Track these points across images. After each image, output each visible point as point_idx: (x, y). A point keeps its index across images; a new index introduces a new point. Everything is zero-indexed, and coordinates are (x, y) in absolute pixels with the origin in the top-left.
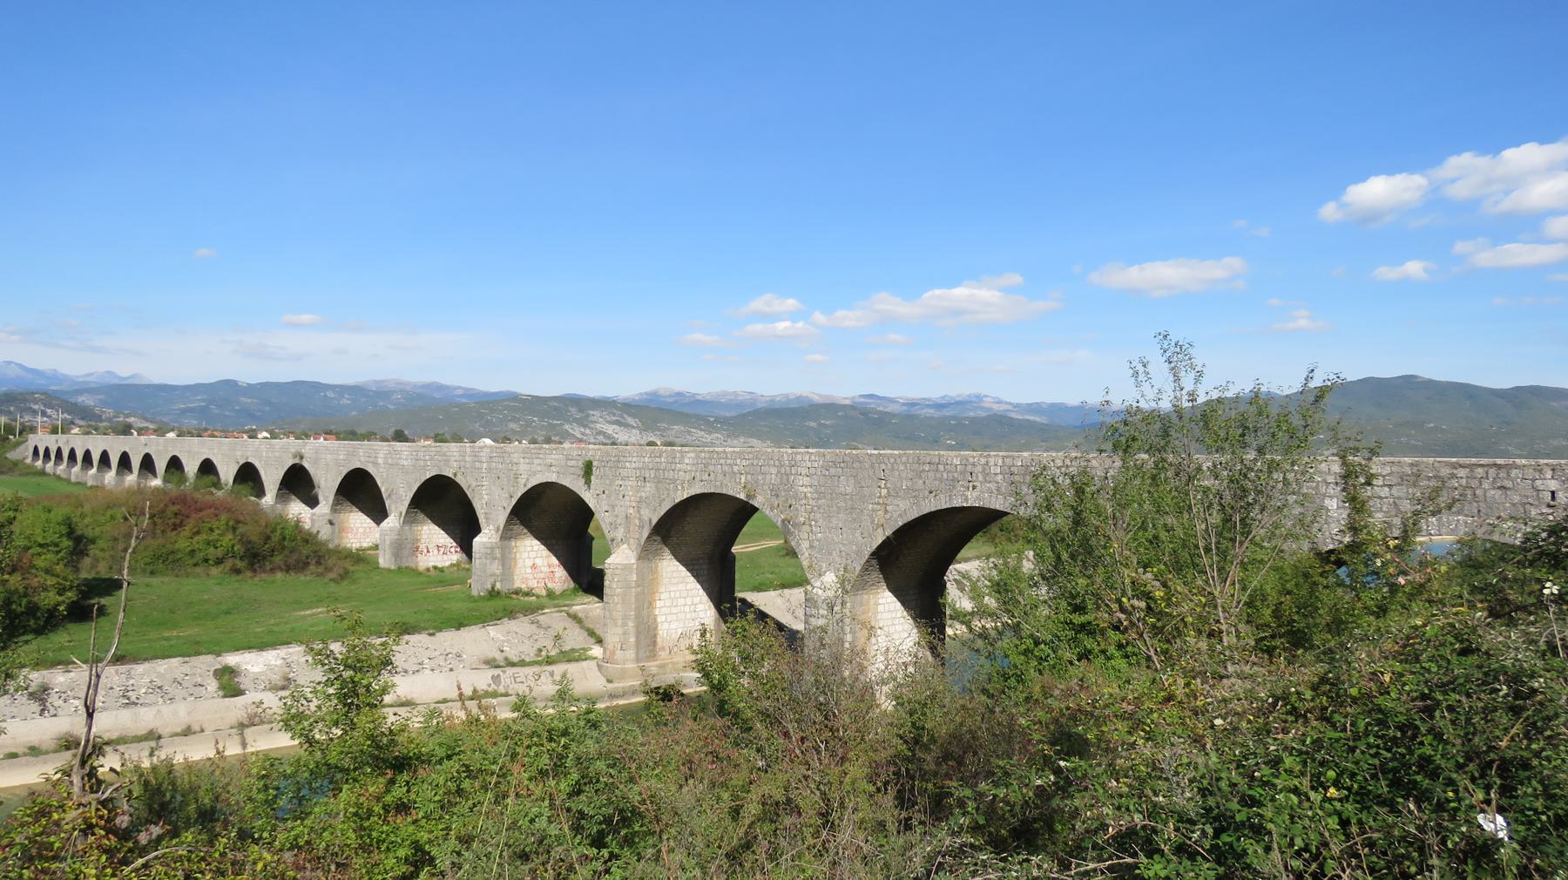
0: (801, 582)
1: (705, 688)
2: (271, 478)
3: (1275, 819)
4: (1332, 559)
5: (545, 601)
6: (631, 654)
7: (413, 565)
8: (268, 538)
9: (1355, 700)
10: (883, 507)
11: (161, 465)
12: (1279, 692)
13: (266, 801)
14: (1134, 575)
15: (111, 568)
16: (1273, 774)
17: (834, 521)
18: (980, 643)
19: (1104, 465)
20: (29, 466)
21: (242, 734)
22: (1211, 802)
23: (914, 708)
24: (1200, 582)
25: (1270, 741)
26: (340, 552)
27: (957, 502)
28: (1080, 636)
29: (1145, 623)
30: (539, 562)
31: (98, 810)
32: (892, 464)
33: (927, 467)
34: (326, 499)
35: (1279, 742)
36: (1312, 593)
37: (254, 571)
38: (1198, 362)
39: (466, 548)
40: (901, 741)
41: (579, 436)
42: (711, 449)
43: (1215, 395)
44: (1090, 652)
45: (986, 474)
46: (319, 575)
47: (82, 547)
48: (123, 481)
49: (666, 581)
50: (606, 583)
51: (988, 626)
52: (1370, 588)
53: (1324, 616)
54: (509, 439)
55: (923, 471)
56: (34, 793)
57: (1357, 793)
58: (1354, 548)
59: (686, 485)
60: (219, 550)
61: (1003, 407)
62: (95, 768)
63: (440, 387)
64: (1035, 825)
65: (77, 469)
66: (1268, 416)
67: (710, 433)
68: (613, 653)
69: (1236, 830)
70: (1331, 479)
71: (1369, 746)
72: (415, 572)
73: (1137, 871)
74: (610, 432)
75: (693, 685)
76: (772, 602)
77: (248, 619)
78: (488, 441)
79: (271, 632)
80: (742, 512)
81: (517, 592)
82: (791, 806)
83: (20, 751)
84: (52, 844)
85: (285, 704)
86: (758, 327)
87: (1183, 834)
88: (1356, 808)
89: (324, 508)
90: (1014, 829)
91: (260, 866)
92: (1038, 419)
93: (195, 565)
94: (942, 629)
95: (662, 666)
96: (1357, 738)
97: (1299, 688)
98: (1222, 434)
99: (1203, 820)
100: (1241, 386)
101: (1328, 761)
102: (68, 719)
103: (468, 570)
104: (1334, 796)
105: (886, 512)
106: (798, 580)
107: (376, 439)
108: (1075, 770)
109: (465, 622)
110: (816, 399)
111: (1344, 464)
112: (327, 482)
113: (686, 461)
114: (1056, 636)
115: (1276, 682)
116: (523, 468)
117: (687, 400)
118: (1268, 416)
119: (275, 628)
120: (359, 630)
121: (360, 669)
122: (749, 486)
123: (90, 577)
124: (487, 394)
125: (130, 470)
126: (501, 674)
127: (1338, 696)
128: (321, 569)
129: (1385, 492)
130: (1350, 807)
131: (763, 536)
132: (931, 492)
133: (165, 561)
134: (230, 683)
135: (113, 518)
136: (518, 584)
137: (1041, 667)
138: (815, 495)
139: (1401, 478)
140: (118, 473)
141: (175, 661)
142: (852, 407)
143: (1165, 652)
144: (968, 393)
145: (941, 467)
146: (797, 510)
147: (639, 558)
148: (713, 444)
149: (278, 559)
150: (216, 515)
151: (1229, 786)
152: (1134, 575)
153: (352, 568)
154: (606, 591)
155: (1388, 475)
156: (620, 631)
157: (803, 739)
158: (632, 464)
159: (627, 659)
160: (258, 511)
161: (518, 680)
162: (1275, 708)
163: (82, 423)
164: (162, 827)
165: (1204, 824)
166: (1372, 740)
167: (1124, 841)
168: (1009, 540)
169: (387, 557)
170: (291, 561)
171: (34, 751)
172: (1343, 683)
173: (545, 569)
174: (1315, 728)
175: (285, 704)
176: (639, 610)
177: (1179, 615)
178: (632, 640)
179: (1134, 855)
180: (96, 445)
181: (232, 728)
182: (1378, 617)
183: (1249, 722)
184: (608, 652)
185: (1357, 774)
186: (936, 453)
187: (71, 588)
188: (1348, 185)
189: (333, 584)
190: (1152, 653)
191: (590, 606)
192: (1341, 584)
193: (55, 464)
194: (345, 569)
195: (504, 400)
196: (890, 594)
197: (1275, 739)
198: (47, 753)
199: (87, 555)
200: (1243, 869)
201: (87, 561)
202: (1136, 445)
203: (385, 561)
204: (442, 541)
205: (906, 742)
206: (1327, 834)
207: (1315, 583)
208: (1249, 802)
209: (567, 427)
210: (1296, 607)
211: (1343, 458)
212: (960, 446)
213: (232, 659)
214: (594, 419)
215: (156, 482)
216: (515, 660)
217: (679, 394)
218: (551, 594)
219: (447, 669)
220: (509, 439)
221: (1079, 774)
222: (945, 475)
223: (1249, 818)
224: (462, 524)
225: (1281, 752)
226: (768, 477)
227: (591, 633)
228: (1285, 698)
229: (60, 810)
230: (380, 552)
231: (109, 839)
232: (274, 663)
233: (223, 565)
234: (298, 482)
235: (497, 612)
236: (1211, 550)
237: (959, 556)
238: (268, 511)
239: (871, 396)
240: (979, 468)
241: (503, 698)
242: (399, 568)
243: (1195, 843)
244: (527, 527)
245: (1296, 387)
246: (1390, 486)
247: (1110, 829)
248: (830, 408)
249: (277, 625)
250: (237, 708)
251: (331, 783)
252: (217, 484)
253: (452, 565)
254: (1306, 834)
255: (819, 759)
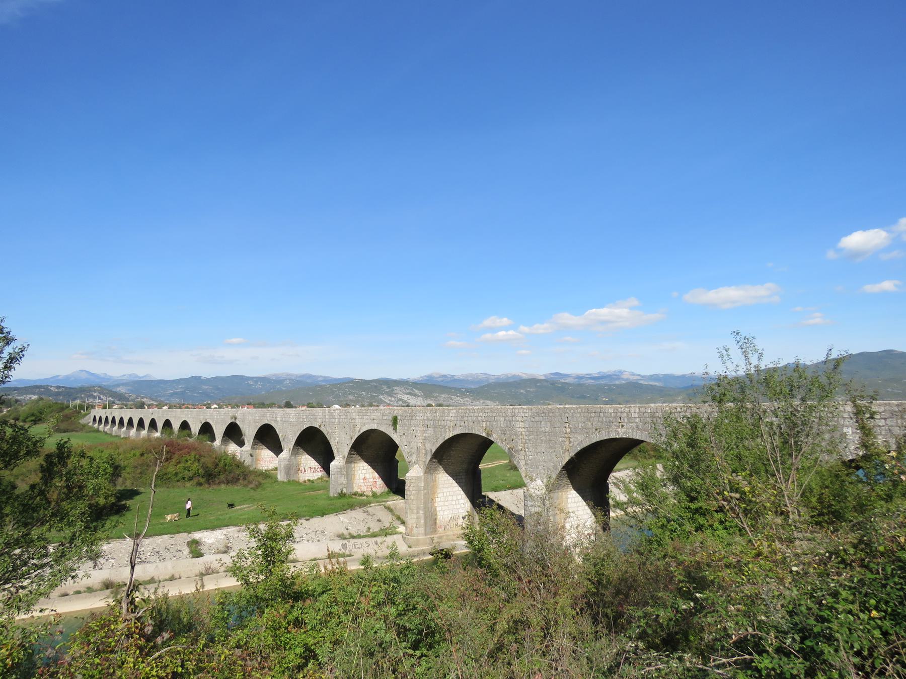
0: (521, 485)
1: (470, 550)
2: (219, 431)
3: (840, 631)
4: (852, 465)
5: (371, 499)
6: (422, 530)
7: (296, 479)
8: (217, 465)
9: (882, 554)
10: (568, 440)
11: (160, 425)
12: (832, 549)
13: (223, 618)
14: (730, 477)
15: (133, 484)
16: (835, 602)
17: (539, 449)
18: (633, 522)
19: (707, 411)
20: (91, 427)
21: (202, 580)
22: (797, 619)
23: (597, 563)
24: (772, 482)
25: (830, 581)
26: (256, 472)
27: (613, 435)
28: (696, 516)
29: (740, 507)
30: (367, 476)
31: (135, 623)
32: (572, 413)
33: (593, 415)
34: (249, 441)
35: (835, 581)
36: (842, 487)
37: (209, 484)
38: (759, 347)
39: (326, 469)
40: (590, 583)
41: (388, 402)
42: (465, 408)
43: (771, 366)
44: (702, 526)
45: (629, 418)
46: (246, 486)
47: (117, 472)
48: (140, 434)
49: (441, 486)
50: (407, 488)
51: (637, 510)
52: (880, 483)
53: (851, 502)
54: (349, 405)
55: (591, 417)
56: (93, 614)
57: (891, 614)
58: (865, 458)
59: (451, 429)
60: (191, 472)
61: (635, 378)
62: (134, 599)
63: (310, 376)
64: (677, 636)
65: (116, 428)
66: (805, 379)
67: (463, 398)
68: (411, 530)
69: (815, 638)
70: (846, 415)
71: (895, 584)
72: (297, 483)
73: (753, 664)
74: (405, 399)
75: (461, 548)
76: (504, 498)
77: (206, 512)
78: (337, 406)
79: (218, 519)
80: (483, 444)
81: (355, 494)
82: (527, 624)
83: (82, 590)
84: (110, 643)
85: (233, 561)
86: (488, 336)
87: (780, 640)
88: (892, 624)
89: (247, 447)
90: (664, 639)
91: (223, 657)
92: (657, 384)
93: (178, 481)
94: (606, 512)
95: (440, 538)
96: (887, 579)
97: (845, 547)
98: (778, 389)
99: (793, 631)
100: (787, 359)
101: (870, 594)
102: (108, 571)
103: (327, 481)
104: (876, 616)
105: (570, 442)
106: (518, 484)
107: (275, 407)
108: (707, 599)
109: (327, 512)
110: (525, 377)
111: (855, 406)
112: (249, 432)
113: (451, 415)
114: (680, 516)
115: (829, 543)
116: (358, 421)
117: (449, 380)
118: (805, 379)
119: (221, 517)
120: (274, 517)
121: (275, 540)
122: (488, 429)
123: (121, 489)
124: (336, 380)
125: (144, 428)
126: (347, 543)
127: (871, 551)
128: (246, 482)
129: (882, 423)
130: (887, 624)
131: (496, 458)
132: (596, 430)
133: (163, 479)
134: (196, 550)
135: (134, 455)
136: (356, 489)
137: (672, 536)
138: (527, 433)
139: (892, 414)
140: (137, 430)
141: (166, 537)
142: (546, 381)
143: (753, 526)
144: (614, 370)
145: (602, 415)
146: (517, 442)
147: (425, 473)
148: (464, 405)
149: (222, 477)
150: (189, 453)
151: (807, 609)
152: (730, 477)
153: (263, 482)
154: (407, 492)
155: (883, 412)
156: (415, 516)
157: (530, 582)
158: (420, 417)
159: (419, 534)
160: (211, 450)
161: (357, 547)
162: (830, 559)
163: (119, 402)
164: (169, 634)
165: (793, 634)
166: (896, 580)
167: (741, 644)
168: (645, 457)
169: (282, 474)
170: (230, 478)
171: (90, 590)
172: (874, 544)
173: (371, 480)
174: (858, 573)
175: (233, 561)
176: (426, 504)
177: (761, 502)
178: (422, 521)
179: (750, 654)
180: (126, 414)
181: (196, 576)
182: (886, 502)
183: (815, 568)
184: (408, 529)
185: (889, 602)
186: (599, 406)
187: (112, 495)
188: (842, 237)
189: (252, 491)
190: (746, 526)
191: (398, 502)
192: (861, 481)
193: (104, 426)
194: (259, 482)
195: (345, 383)
196: (575, 492)
197: (833, 580)
198: (96, 591)
199: (120, 476)
200: (821, 664)
201: (120, 480)
202: (726, 399)
203: (281, 477)
204: (312, 464)
205: (593, 583)
206: (874, 641)
207: (843, 481)
208: (822, 619)
209: (381, 397)
210: (833, 496)
211: (854, 402)
212: (611, 402)
213: (197, 535)
214: (397, 392)
215: (157, 434)
216: (355, 534)
217: (445, 376)
218: (374, 495)
219: (316, 540)
220: (349, 405)
221: (710, 602)
222: (604, 419)
223: (822, 630)
224: (324, 454)
225: (838, 588)
226: (499, 423)
227: (399, 518)
228: (837, 553)
229: (115, 623)
230: (278, 472)
231: (141, 641)
232: (219, 537)
233: (192, 481)
234: (233, 432)
235: (344, 506)
236: (777, 461)
237: (615, 468)
238: (218, 449)
239: (556, 374)
240: (625, 415)
241: (348, 558)
242: (289, 481)
243: (789, 646)
244: (360, 455)
245: (822, 358)
246: (885, 419)
247: (734, 637)
248: (533, 382)
249: (222, 515)
250: (199, 564)
251: (258, 608)
252: (190, 435)
253: (319, 479)
254: (860, 641)
255: (540, 594)
